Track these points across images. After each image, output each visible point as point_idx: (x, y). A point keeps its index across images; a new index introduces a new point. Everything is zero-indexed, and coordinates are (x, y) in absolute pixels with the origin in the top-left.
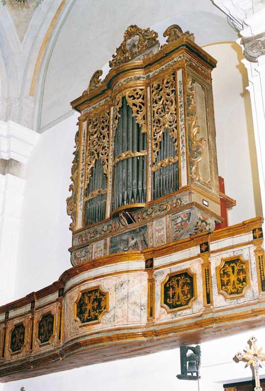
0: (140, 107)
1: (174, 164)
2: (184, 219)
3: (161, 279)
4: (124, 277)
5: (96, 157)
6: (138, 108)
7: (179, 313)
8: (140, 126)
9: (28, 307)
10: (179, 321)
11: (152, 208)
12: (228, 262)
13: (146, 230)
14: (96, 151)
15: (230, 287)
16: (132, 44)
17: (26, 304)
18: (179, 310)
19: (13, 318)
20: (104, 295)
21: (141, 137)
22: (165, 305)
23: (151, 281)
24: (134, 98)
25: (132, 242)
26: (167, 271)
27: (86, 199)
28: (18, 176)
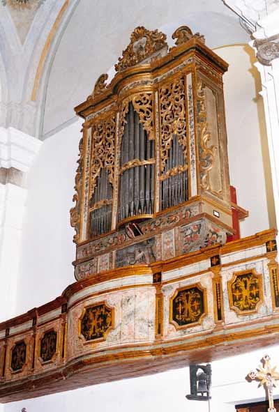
0: (148, 113)
1: (183, 173)
2: (194, 231)
3: (169, 294)
4: (131, 292)
5: (102, 166)
6: (145, 114)
7: (188, 330)
8: (148, 133)
9: (29, 324)
10: (189, 338)
11: (160, 220)
12: (241, 276)
13: (154, 243)
14: (101, 159)
15: (242, 303)
16: (139, 46)
17: (28, 320)
18: (188, 327)
19: (14, 335)
20: (109, 310)
21: (149, 145)
22: (173, 322)
23: (159, 296)
24: (142, 104)
25: (139, 256)
26: (176, 286)
27: (91, 210)
28: (19, 186)
